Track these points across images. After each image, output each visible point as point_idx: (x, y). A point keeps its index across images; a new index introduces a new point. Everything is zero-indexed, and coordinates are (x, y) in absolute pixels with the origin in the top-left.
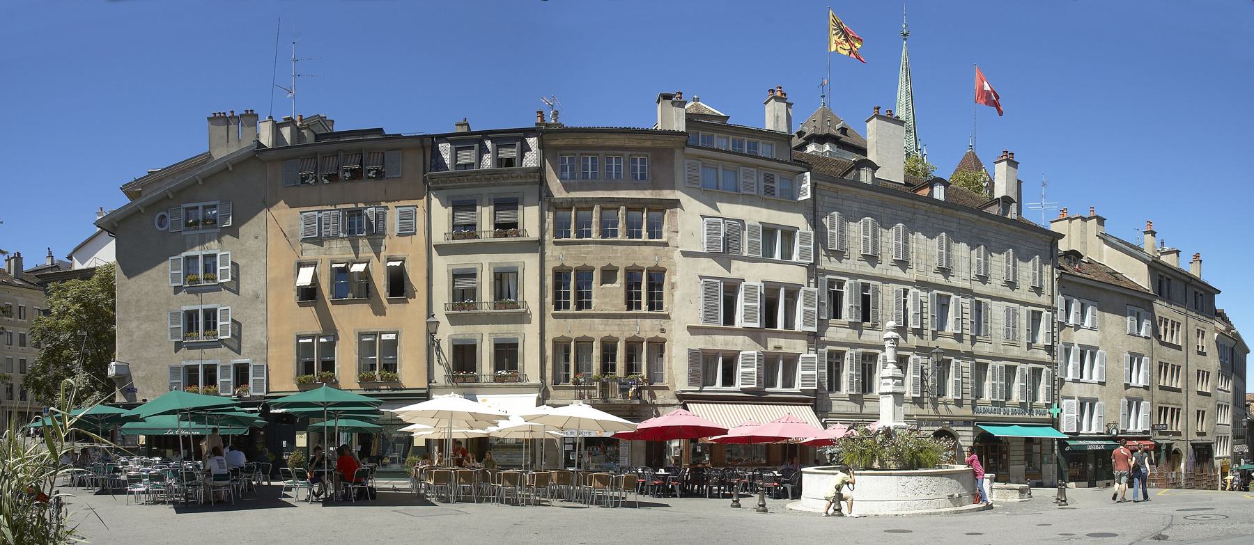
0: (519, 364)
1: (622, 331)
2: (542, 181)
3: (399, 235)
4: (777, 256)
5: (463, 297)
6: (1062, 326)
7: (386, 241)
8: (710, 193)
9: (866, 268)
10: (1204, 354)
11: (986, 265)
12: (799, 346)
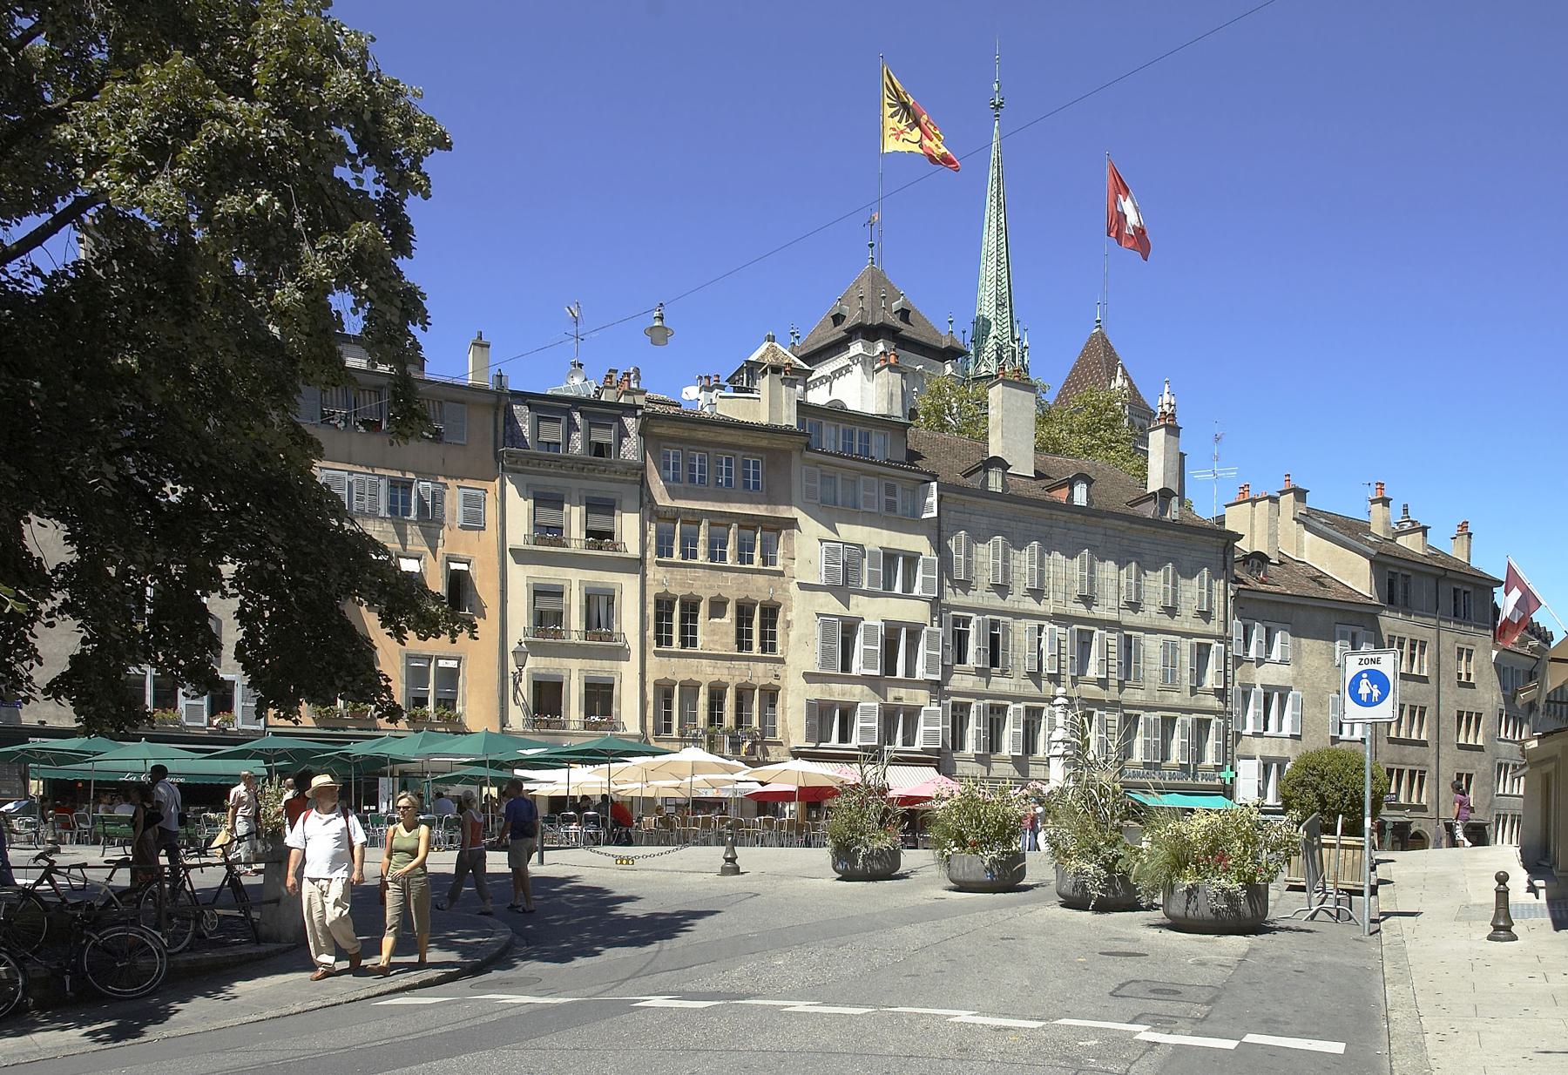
0: (615, 710)
1: (731, 675)
2: (643, 483)
3: (463, 527)
4: (898, 589)
5: (547, 619)
6: (1239, 661)
7: (444, 533)
8: (830, 510)
9: (995, 601)
10: (1472, 686)
11: (1138, 587)
12: (921, 697)
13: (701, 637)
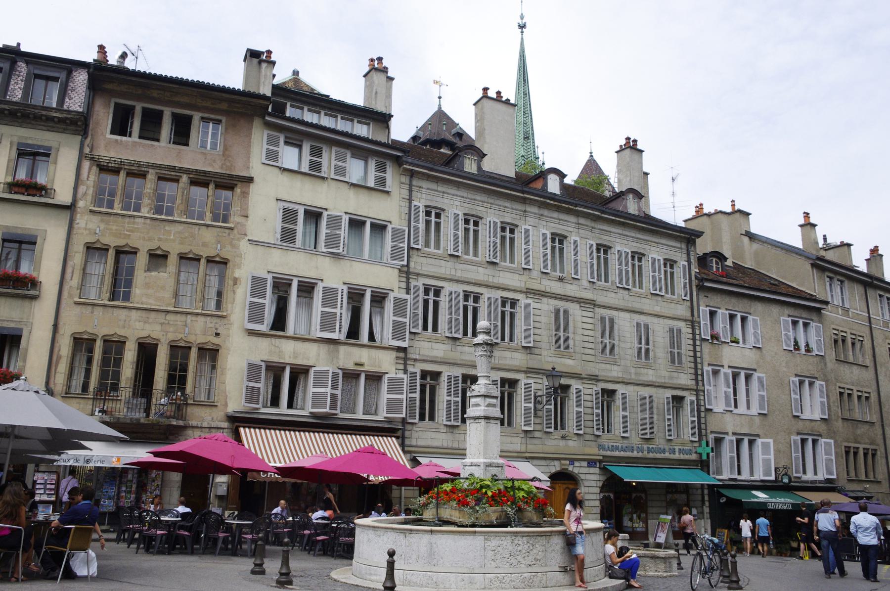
1: (164, 333)
13: (137, 291)
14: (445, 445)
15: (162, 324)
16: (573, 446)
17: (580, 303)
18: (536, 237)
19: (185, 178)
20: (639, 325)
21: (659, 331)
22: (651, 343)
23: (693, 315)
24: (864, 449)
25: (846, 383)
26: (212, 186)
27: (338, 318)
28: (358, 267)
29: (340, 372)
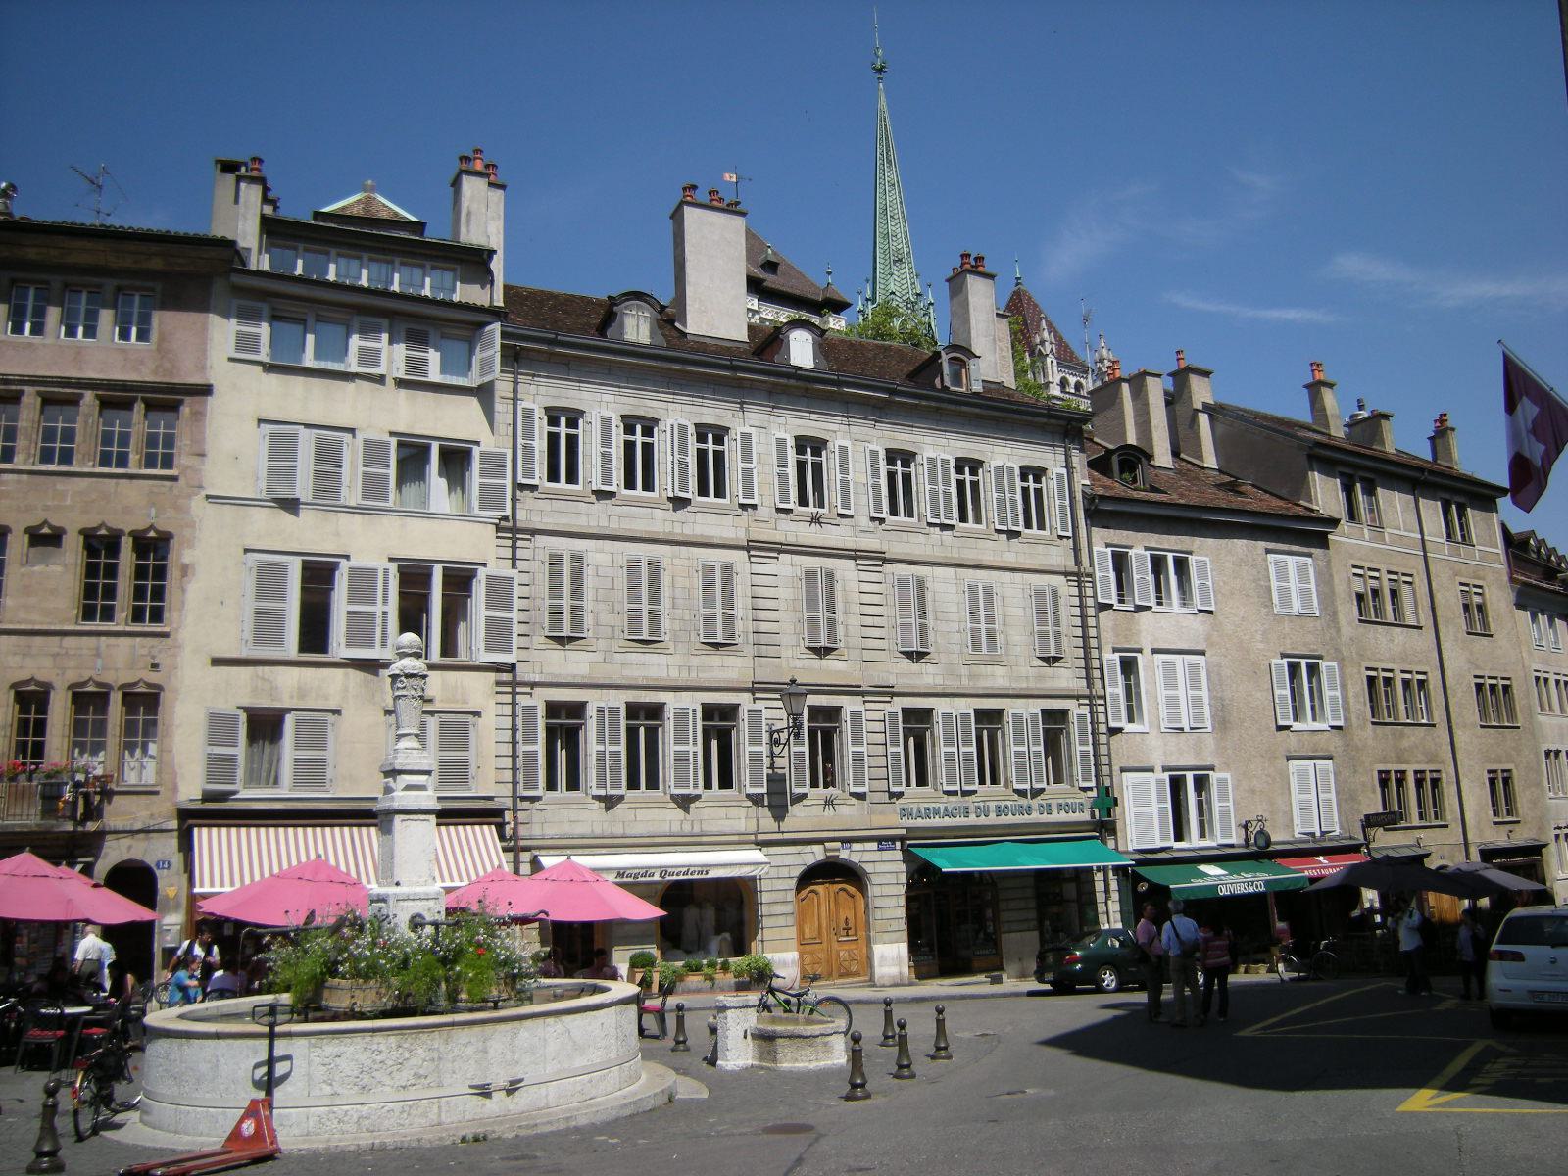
14: (598, 831)
15: (55, 655)
16: (850, 815)
17: (855, 558)
18: (763, 448)
19: (89, 397)
20: (973, 589)
21: (1014, 596)
22: (998, 618)
23: (1078, 562)
24: (1416, 772)
25: (1380, 660)
26: (139, 408)
27: (379, 621)
28: (417, 527)
29: (241, 712)
